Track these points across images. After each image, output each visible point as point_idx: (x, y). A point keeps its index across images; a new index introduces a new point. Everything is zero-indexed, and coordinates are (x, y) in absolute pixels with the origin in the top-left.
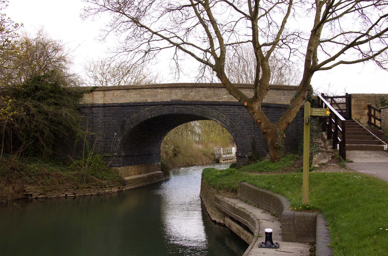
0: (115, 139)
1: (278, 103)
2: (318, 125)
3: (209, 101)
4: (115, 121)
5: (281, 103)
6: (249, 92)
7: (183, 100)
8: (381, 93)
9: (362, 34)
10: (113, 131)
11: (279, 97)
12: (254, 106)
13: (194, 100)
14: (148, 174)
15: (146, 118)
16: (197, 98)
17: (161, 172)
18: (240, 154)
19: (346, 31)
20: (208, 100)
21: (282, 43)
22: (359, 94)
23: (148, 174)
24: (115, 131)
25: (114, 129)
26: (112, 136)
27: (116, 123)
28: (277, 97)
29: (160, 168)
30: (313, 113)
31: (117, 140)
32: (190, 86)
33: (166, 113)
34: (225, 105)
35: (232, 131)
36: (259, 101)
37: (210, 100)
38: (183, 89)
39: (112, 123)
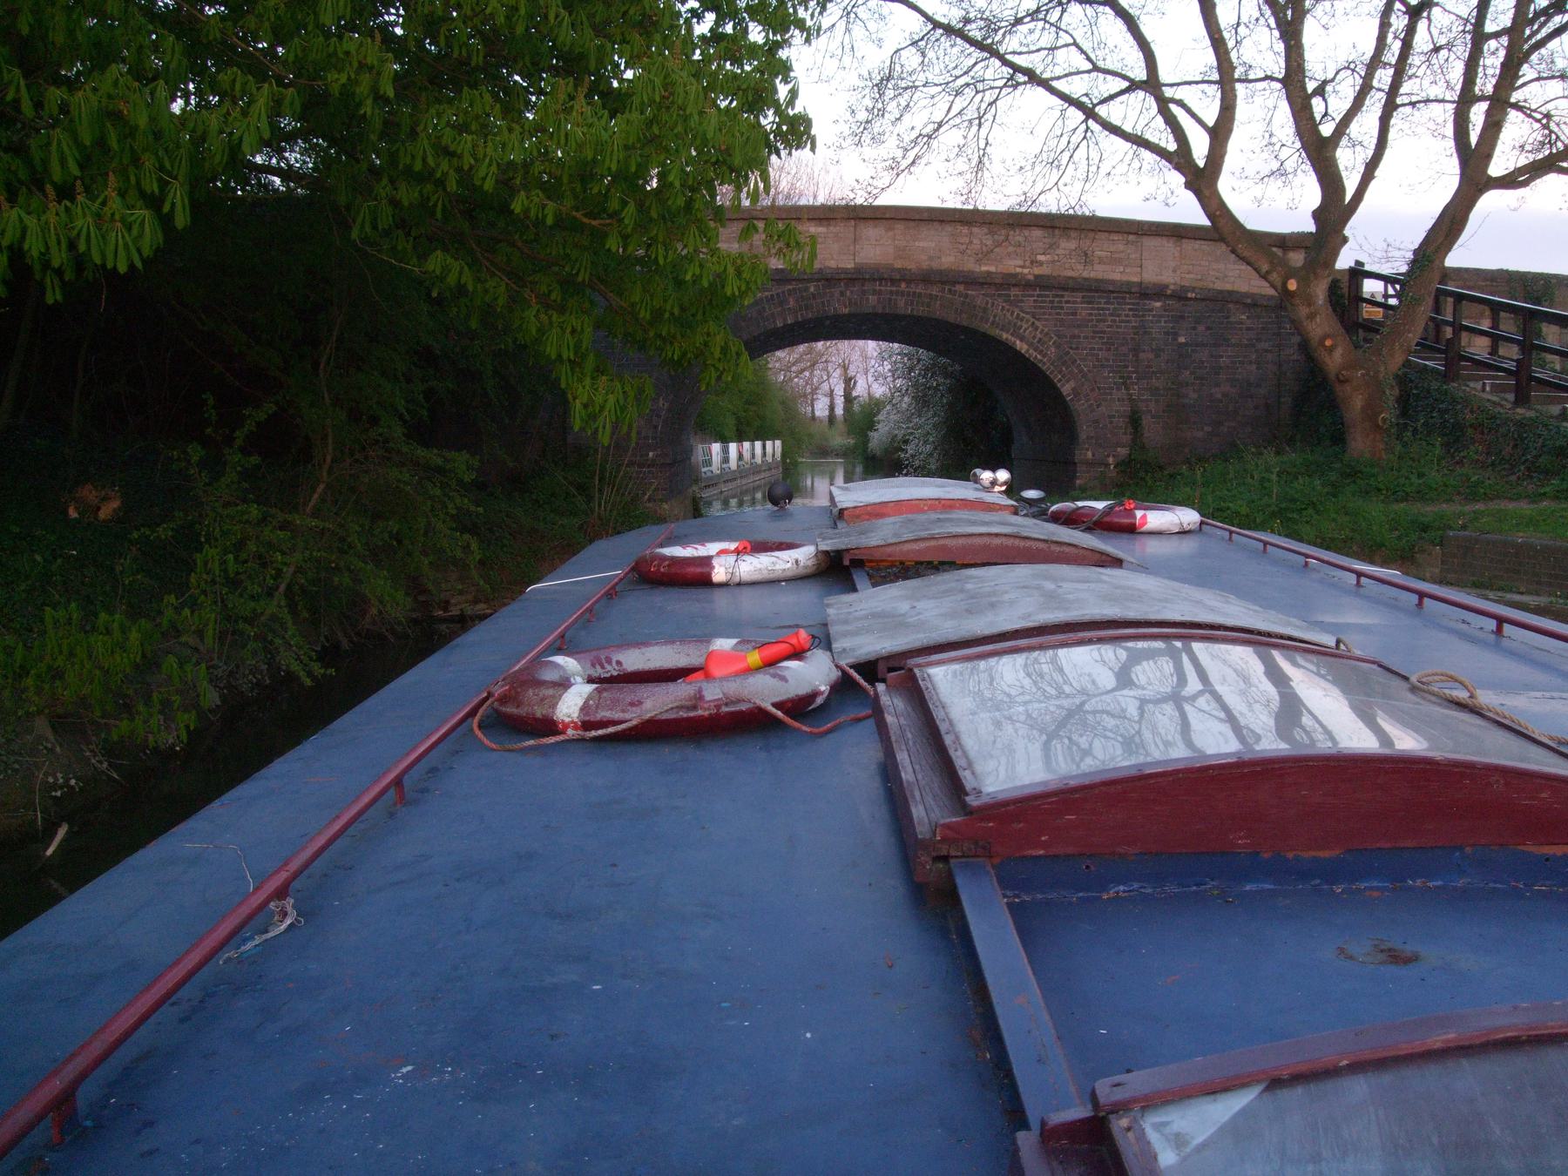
1: (1219, 286)
2: (809, 35)
3: (989, 273)
5: (1228, 287)
6: (1121, 247)
7: (898, 264)
8: (1512, 268)
9: (1350, 187)
11: (1221, 266)
13: (935, 265)
16: (948, 261)
19: (1396, 121)
20: (984, 268)
21: (1242, 111)
22: (1467, 270)
28: (1215, 266)
32: (925, 216)
34: (1043, 288)
37: (992, 269)
38: (900, 226)
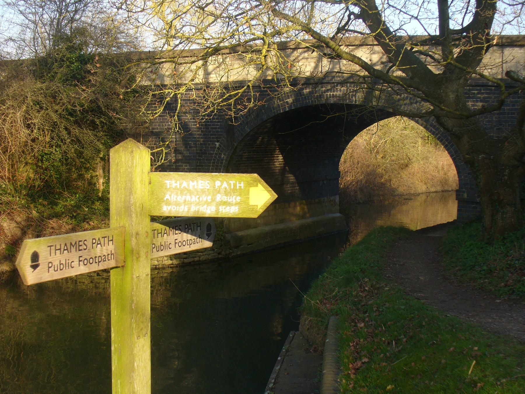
0: (216, 154)
4: (217, 119)
10: (213, 138)
12: (444, 95)
14: (315, 219)
15: (274, 112)
17: (338, 215)
18: (465, 195)
23: (315, 219)
24: (216, 138)
25: (215, 135)
26: (211, 148)
27: (218, 122)
29: (338, 208)
30: (168, 203)
31: (220, 157)
33: (312, 101)
35: (449, 143)
36: (459, 79)
39: (211, 122)
